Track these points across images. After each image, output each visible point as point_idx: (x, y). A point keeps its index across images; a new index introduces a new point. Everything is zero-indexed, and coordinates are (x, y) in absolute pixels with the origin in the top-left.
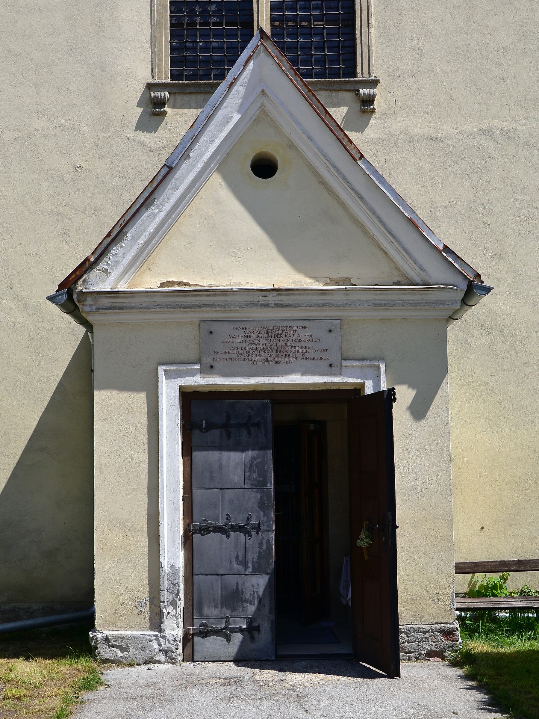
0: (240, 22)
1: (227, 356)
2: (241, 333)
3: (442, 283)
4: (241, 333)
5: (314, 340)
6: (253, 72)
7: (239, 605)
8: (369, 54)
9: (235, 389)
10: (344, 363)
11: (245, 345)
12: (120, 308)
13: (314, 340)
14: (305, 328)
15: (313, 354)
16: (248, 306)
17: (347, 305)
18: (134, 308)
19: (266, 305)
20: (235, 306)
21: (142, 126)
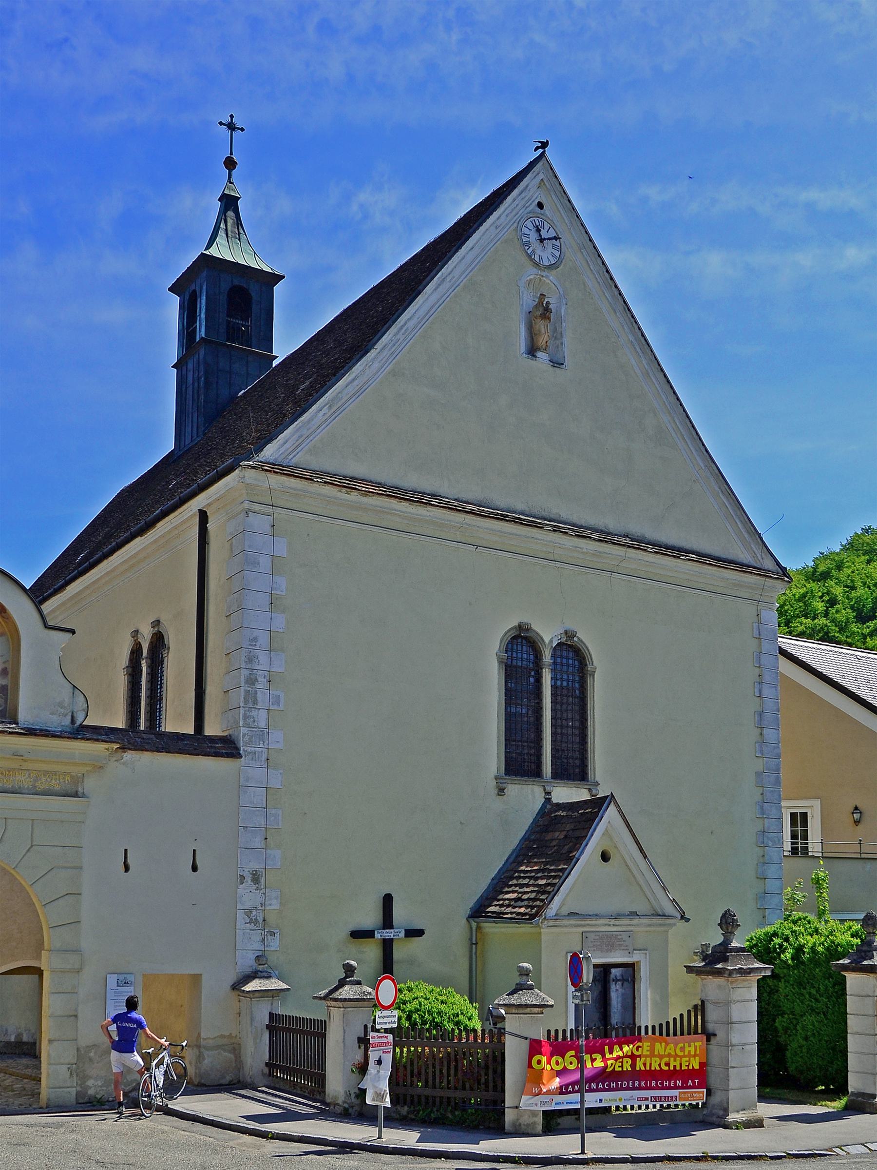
0: (554, 687)
1: (593, 949)
2: (598, 937)
3: (794, 1160)
4: (598, 937)
5: (624, 941)
6: (231, 462)
7: (587, 1038)
8: (208, 1124)
9: (715, 570)
10: (635, 951)
11: (599, 943)
12: (556, 926)
13: (624, 941)
14: (621, 935)
15: (623, 948)
16: (603, 925)
17: (638, 925)
18: (561, 926)
19: (610, 925)
20: (598, 925)
21: (125, 872)
